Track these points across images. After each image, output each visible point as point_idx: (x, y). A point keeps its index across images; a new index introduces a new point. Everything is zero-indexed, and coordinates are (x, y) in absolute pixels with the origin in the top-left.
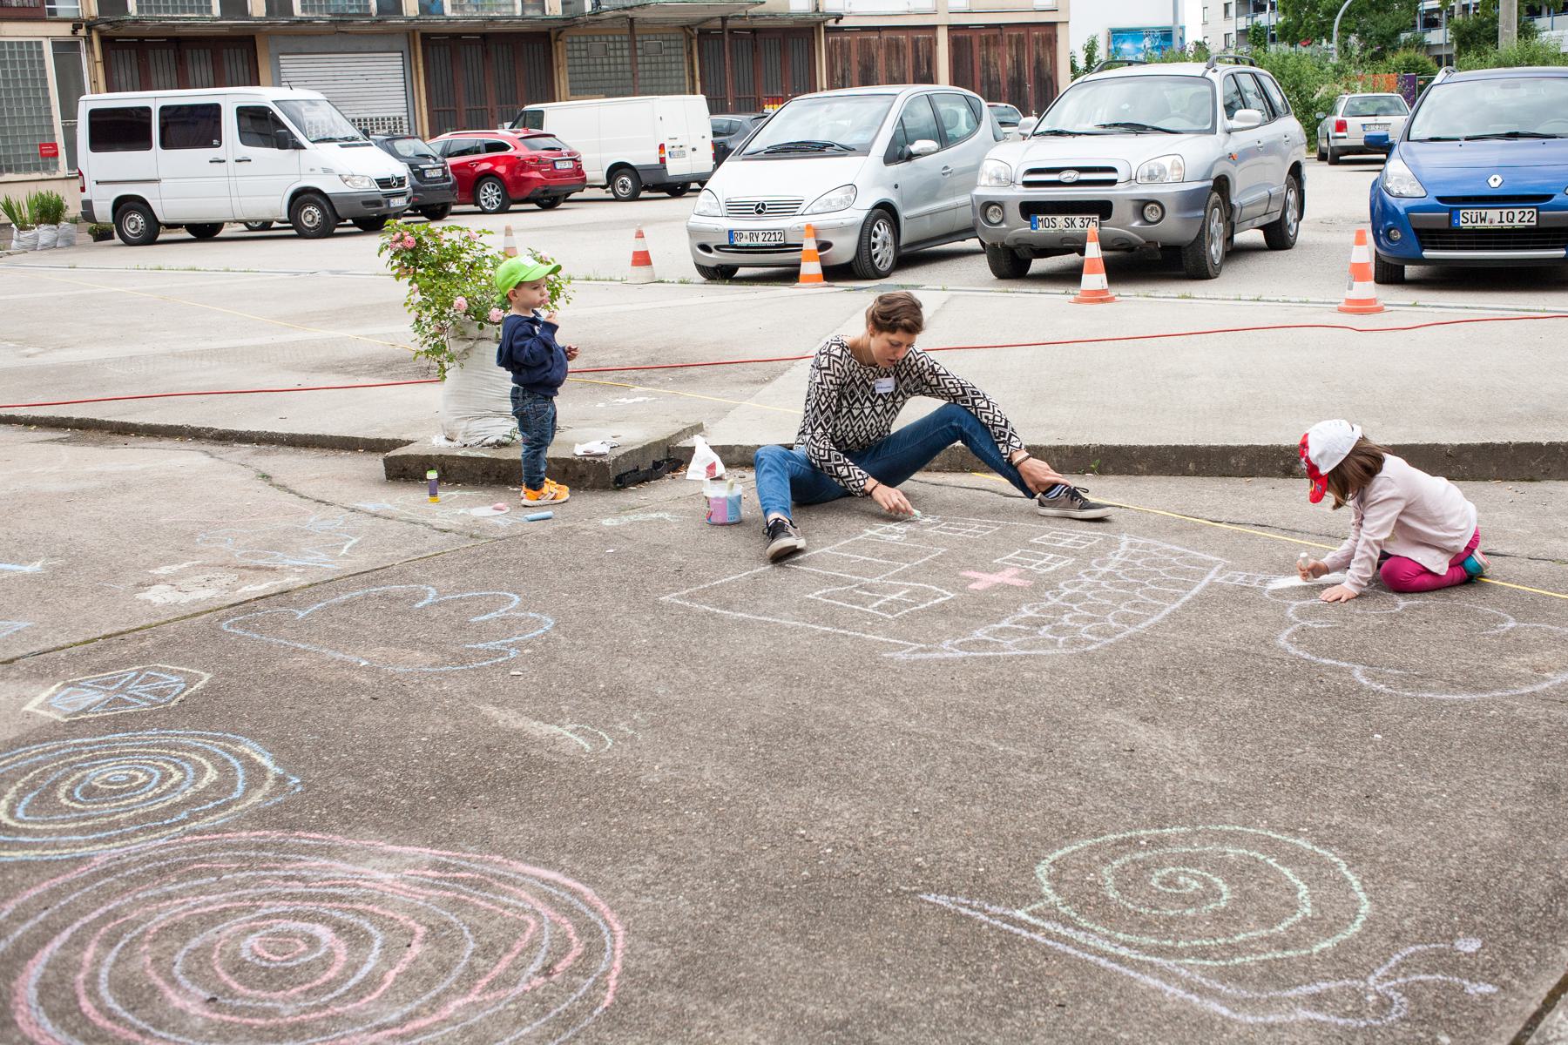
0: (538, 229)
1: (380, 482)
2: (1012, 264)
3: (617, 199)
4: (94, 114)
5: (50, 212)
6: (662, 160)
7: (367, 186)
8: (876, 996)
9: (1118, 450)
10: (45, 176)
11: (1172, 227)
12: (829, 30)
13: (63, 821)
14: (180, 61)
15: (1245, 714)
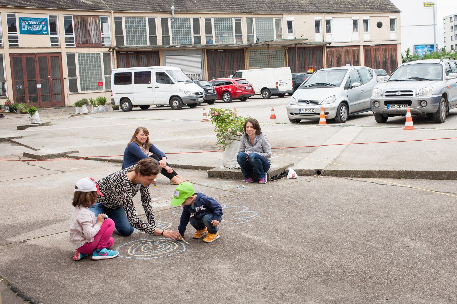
0: (241, 107)
1: (206, 178)
2: (382, 119)
3: (264, 98)
4: (116, 74)
5: (102, 102)
6: (277, 87)
7: (192, 95)
8: (343, 296)
9: (410, 172)
10: (99, 91)
11: (430, 108)
12: (327, 47)
13: (144, 255)
14: (138, 58)
15: (439, 239)
